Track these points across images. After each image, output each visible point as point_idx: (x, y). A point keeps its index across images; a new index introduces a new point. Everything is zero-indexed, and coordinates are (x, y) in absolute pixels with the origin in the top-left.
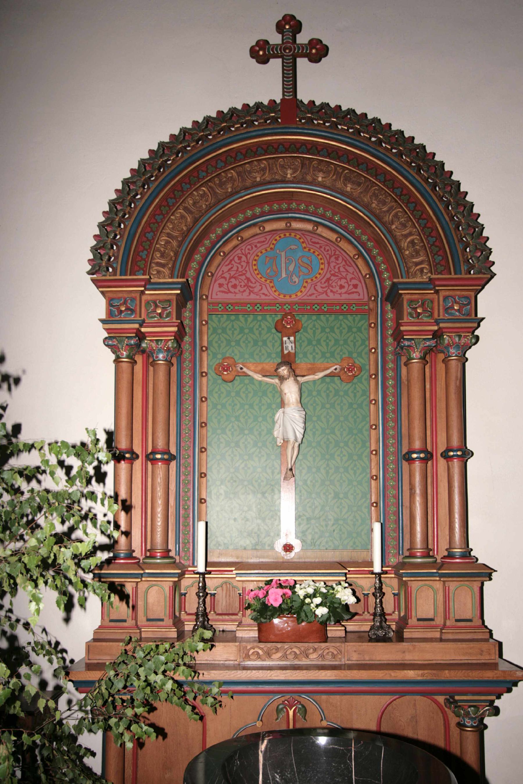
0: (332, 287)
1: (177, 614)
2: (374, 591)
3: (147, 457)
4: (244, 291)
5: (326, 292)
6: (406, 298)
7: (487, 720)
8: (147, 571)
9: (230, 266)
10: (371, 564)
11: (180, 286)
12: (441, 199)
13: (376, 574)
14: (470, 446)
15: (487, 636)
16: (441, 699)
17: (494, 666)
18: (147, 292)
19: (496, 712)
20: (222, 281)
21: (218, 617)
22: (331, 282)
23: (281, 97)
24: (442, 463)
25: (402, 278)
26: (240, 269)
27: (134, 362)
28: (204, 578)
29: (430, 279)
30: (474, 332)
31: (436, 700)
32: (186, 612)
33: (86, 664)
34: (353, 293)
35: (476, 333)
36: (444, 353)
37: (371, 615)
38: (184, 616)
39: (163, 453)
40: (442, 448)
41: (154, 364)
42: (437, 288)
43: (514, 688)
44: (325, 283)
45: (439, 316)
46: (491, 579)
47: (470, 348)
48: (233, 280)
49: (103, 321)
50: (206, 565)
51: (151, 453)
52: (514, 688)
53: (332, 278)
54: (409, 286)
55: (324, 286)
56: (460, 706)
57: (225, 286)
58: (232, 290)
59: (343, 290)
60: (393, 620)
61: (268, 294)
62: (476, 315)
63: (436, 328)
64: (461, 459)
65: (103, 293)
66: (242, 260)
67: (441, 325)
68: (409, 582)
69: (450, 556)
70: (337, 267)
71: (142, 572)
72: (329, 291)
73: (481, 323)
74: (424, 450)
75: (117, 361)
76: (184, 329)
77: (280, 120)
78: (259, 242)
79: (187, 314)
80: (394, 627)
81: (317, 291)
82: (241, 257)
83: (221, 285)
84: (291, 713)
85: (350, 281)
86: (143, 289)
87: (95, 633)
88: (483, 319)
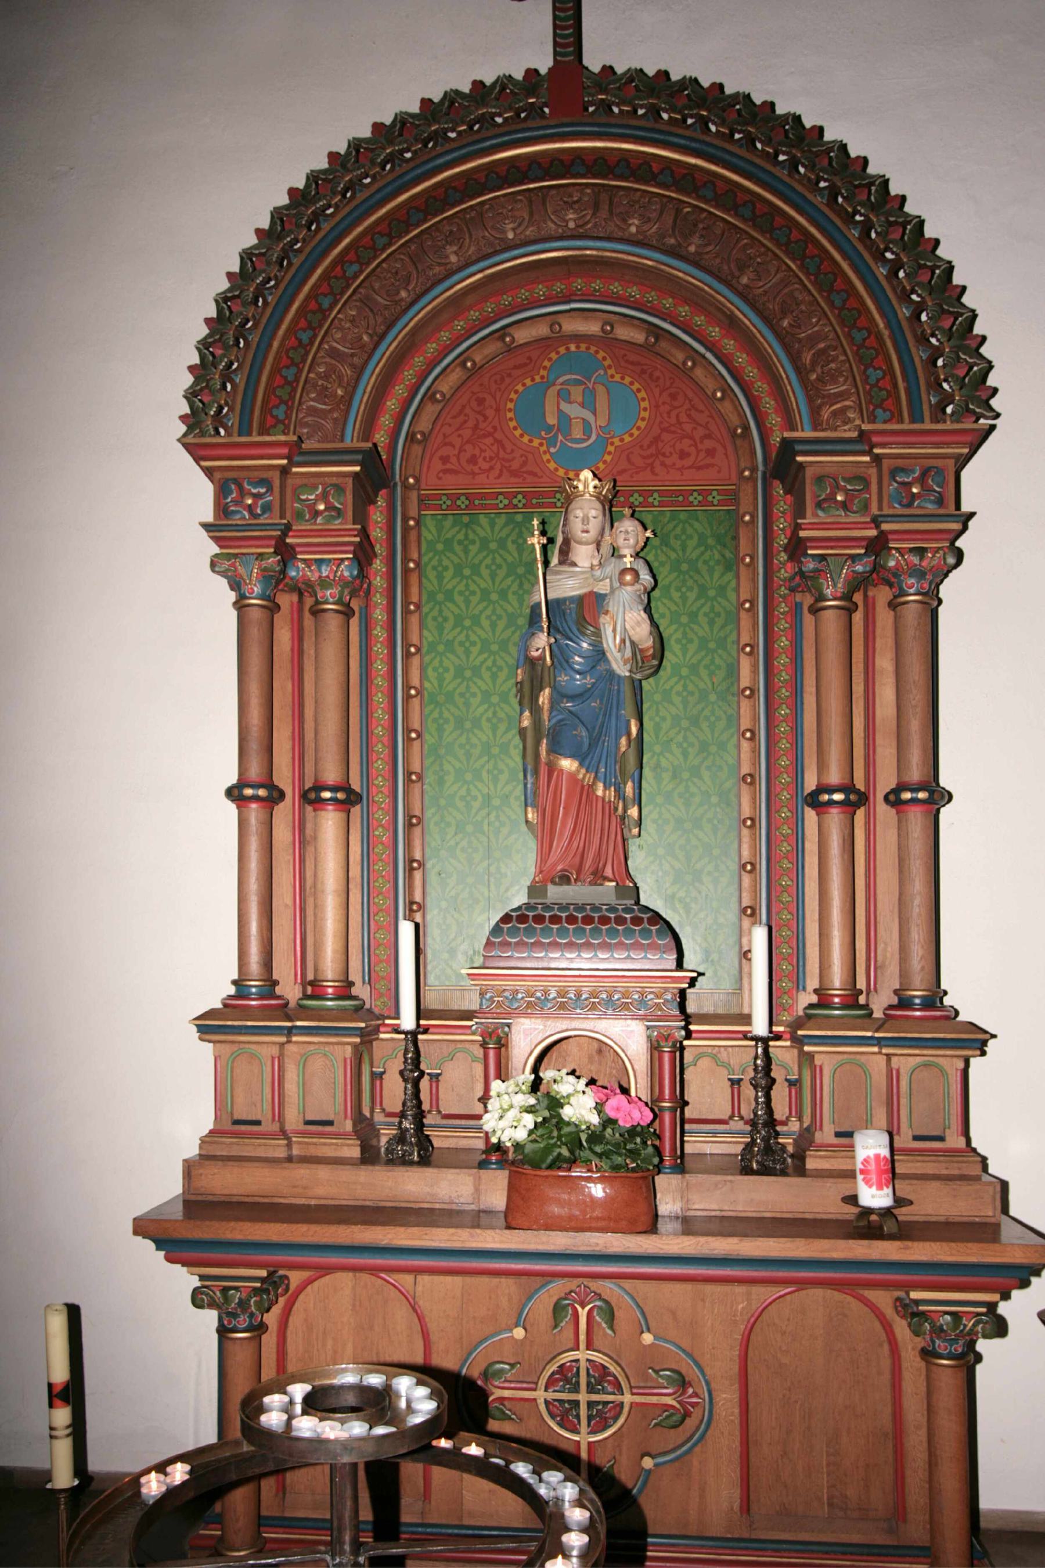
0: (664, 455)
1: (366, 1112)
2: (752, 1074)
3: (304, 796)
4: (492, 468)
5: (652, 465)
6: (809, 473)
7: (982, 1345)
8: (299, 1023)
9: (462, 418)
10: (747, 1019)
11: (360, 457)
12: (849, 219)
13: (756, 1039)
14: (945, 780)
15: (977, 1170)
16: (883, 1299)
17: (986, 1232)
18: (294, 470)
19: (1000, 1328)
20: (445, 451)
21: (445, 1122)
22: (661, 445)
23: (550, 63)
24: (883, 811)
25: (803, 430)
26: (482, 425)
27: (272, 608)
28: (415, 1042)
29: (862, 434)
30: (953, 543)
31: (866, 1298)
32: (383, 1110)
33: (184, 1201)
34: (707, 466)
35: (958, 544)
36: (891, 585)
37: (746, 1123)
38: (379, 1117)
39: (334, 789)
40: (886, 781)
41: (317, 612)
42: (876, 451)
43: (1034, 1280)
44: (649, 447)
45: (880, 508)
46: (983, 1053)
47: (946, 576)
48: (468, 447)
49: (206, 526)
50: (419, 1014)
51: (310, 789)
52: (1034, 1280)
53: (666, 436)
54: (818, 446)
55: (649, 452)
56: (923, 1313)
57: (454, 460)
58: (469, 468)
59: (688, 462)
60: (787, 1135)
61: (540, 474)
62: (958, 506)
63: (873, 533)
64: (926, 807)
65: (209, 472)
66: (487, 403)
67: (885, 527)
68: (816, 1056)
69: (905, 1003)
70: (674, 414)
71: (289, 1024)
72: (657, 463)
73: (971, 523)
74: (847, 788)
75: (240, 605)
76: (372, 547)
77: (547, 110)
78: (516, 367)
79: (377, 516)
80: (790, 1149)
81: (633, 464)
82: (484, 400)
83: (445, 460)
84: (583, 1313)
85: (701, 442)
86: (285, 462)
87: (203, 1141)
88: (972, 515)
